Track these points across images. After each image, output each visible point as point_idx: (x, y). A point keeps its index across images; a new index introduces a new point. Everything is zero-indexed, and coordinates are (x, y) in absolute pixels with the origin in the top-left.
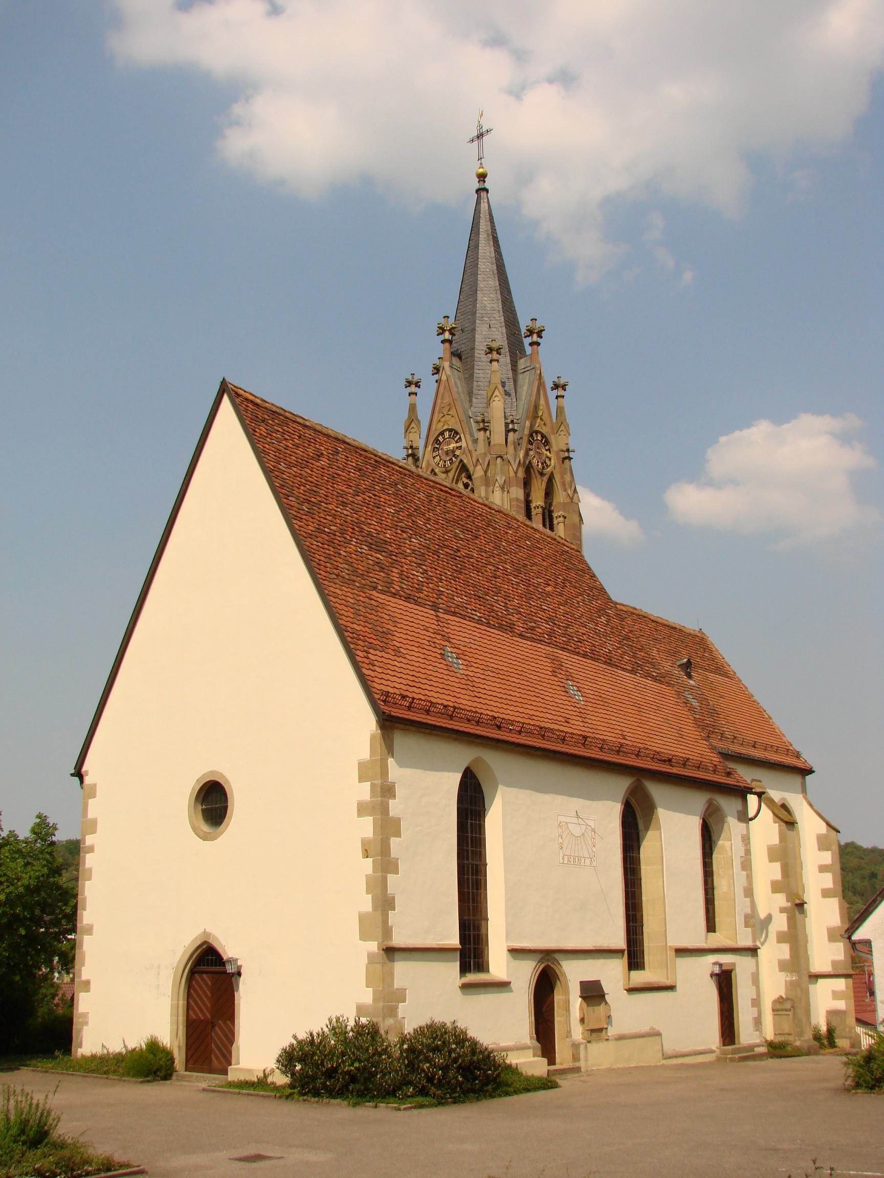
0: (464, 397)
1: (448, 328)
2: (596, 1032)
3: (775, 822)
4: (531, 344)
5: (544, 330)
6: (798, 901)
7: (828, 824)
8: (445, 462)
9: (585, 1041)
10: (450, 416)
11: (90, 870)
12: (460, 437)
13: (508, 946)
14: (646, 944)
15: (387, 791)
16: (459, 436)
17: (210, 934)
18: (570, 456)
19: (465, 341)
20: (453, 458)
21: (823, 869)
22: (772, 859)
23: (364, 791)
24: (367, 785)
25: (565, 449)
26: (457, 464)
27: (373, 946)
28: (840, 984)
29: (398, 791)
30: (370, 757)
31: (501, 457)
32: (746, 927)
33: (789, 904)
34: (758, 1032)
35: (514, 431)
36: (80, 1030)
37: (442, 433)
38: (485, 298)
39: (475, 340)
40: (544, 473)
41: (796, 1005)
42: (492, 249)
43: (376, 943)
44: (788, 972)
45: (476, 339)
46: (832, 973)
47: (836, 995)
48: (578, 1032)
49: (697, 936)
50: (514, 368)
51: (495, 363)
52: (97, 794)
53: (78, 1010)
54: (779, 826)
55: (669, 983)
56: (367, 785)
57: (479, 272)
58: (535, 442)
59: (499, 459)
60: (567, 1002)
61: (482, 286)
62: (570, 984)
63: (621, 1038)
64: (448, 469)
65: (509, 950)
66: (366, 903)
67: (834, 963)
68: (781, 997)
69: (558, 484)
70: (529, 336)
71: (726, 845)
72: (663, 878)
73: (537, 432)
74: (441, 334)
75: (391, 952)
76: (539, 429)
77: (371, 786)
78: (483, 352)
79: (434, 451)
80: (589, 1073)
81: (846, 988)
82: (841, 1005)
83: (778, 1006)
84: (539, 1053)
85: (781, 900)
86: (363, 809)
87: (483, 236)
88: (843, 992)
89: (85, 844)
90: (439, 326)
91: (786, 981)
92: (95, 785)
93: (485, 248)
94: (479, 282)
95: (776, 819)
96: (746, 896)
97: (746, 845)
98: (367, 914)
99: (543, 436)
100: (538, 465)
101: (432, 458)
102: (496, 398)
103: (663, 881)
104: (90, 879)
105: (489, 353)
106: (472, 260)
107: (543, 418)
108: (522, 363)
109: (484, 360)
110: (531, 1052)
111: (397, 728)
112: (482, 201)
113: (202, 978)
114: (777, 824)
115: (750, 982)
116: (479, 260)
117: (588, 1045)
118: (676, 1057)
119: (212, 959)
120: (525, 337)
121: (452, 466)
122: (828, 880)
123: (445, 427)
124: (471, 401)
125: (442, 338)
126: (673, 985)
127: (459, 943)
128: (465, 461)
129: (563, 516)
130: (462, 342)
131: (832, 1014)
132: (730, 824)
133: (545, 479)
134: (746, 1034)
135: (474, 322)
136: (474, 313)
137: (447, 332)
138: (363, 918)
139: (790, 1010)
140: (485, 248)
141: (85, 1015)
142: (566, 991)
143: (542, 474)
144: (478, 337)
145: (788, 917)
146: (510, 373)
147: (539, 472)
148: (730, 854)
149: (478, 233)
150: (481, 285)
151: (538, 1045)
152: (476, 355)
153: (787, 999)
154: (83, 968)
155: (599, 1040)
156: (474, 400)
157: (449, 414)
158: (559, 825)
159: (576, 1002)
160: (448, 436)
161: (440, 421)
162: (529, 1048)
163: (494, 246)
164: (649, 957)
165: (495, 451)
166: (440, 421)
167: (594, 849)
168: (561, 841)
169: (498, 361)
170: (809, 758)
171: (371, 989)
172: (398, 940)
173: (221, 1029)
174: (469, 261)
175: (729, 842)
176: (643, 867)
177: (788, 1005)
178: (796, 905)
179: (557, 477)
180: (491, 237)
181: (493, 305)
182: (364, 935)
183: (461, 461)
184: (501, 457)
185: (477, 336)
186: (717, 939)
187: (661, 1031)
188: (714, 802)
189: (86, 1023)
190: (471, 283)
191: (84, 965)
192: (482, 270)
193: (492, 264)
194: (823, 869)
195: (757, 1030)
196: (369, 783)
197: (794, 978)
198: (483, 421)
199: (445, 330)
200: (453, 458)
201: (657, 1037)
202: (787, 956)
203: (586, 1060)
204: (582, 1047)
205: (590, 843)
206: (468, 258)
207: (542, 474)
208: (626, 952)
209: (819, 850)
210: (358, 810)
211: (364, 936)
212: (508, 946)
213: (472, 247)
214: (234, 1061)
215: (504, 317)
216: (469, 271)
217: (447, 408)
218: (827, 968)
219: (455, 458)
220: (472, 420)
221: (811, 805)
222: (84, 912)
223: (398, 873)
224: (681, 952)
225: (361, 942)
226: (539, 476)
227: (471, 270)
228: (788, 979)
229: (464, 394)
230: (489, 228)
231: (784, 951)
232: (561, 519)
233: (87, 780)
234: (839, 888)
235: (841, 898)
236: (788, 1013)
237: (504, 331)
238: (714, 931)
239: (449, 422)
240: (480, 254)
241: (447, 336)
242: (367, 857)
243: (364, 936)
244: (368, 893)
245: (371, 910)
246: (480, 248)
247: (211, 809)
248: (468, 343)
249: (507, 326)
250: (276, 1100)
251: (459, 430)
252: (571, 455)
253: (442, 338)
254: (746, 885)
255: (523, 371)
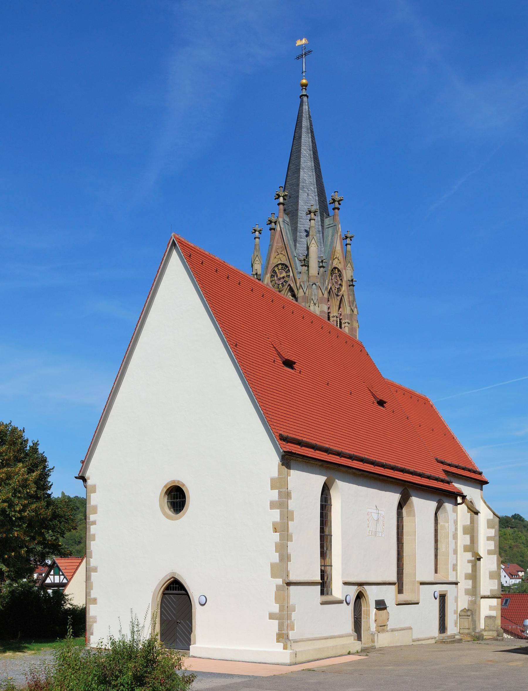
0: (292, 243)
1: (283, 195)
2: (382, 627)
3: (468, 512)
4: (334, 209)
5: (343, 200)
6: (478, 557)
7: (494, 514)
8: (278, 285)
9: (377, 632)
10: (282, 255)
11: (94, 535)
12: (289, 269)
13: (343, 581)
14: (404, 580)
15: (286, 495)
16: (288, 269)
17: (176, 573)
18: (353, 284)
19: (292, 204)
20: (284, 283)
21: (489, 539)
22: (465, 533)
23: (274, 495)
24: (276, 491)
25: (350, 279)
26: (287, 287)
27: (280, 581)
28: (495, 602)
29: (293, 495)
30: (278, 476)
31: (315, 284)
32: (453, 571)
33: (473, 558)
34: (456, 628)
35: (323, 267)
36: (91, 626)
37: (277, 266)
38: (305, 175)
39: (298, 204)
40: (339, 295)
41: (473, 613)
42: (310, 140)
43: (281, 580)
44: (470, 595)
45: (299, 204)
46: (490, 596)
47: (491, 608)
48: (373, 627)
49: (430, 577)
50: (322, 224)
51: (312, 221)
52: (96, 491)
53: (89, 614)
54: (471, 515)
55: (415, 600)
56: (276, 491)
57: (301, 156)
58: (334, 274)
59: (314, 285)
60: (368, 611)
61: (303, 166)
62: (370, 601)
63: (393, 630)
64: (280, 290)
65: (343, 583)
66: (275, 558)
67: (491, 591)
68: (465, 609)
69: (346, 301)
70: (332, 203)
71: (446, 525)
72: (415, 543)
73: (335, 268)
74: (277, 198)
75: (289, 584)
76: (337, 266)
77: (279, 492)
78: (305, 213)
79: (271, 277)
80: (381, 649)
81: (497, 604)
82: (493, 613)
83: (463, 614)
84: (356, 638)
85: (469, 556)
86: (273, 505)
87: (304, 130)
88: (495, 606)
89: (90, 520)
90: (277, 193)
91: (468, 600)
92: (95, 486)
93: (306, 139)
94: (301, 163)
95: (469, 510)
96: (454, 554)
97: (456, 525)
98: (276, 563)
99: (339, 270)
100: (335, 290)
101: (270, 282)
102: (313, 245)
103: (415, 545)
104: (94, 540)
105: (309, 214)
106: (297, 147)
107: (339, 258)
108: (327, 221)
109: (304, 218)
110: (352, 638)
111: (292, 459)
112: (304, 104)
113: (170, 597)
114: (470, 513)
115: (454, 601)
116: (302, 147)
117: (379, 634)
118: (418, 641)
119: (176, 587)
120: (330, 203)
121: (283, 288)
122: (492, 545)
123: (279, 262)
124: (295, 246)
125: (277, 201)
126: (418, 602)
127: (320, 579)
128: (292, 285)
129: (348, 323)
130: (290, 205)
131: (488, 618)
132: (449, 514)
133: (339, 298)
134: (452, 629)
135: (298, 192)
136: (298, 185)
137: (281, 197)
138: (273, 566)
139: (470, 616)
140: (306, 139)
141: (95, 617)
142: (368, 605)
143: (337, 295)
144: (301, 202)
145: (472, 565)
146: (320, 227)
147: (336, 294)
148: (448, 530)
149: (301, 127)
150: (303, 165)
151: (356, 634)
152: (299, 214)
153: (468, 610)
154: (92, 591)
155: (383, 631)
156: (297, 244)
157: (282, 254)
158: (368, 514)
159: (373, 610)
160: (281, 268)
161: (275, 258)
162: (352, 636)
163: (311, 137)
164: (406, 587)
165: (312, 280)
166: (275, 258)
167: (384, 527)
168: (368, 523)
169: (314, 220)
170: (486, 476)
171: (278, 605)
172: (293, 578)
173: (183, 625)
174: (295, 148)
175: (448, 524)
176: (404, 537)
177: (469, 613)
178: (477, 559)
179: (346, 297)
180: (310, 131)
181: (311, 180)
182: (274, 575)
183: (289, 285)
184: (315, 284)
185: (300, 201)
186: (440, 577)
187: (412, 627)
188: (442, 501)
189: (96, 622)
190: (296, 163)
191: (92, 589)
192: (304, 154)
193: (310, 151)
194: (489, 539)
195: (456, 627)
196: (278, 490)
197: (473, 599)
198: (352, 280)
199: (280, 196)
200: (284, 283)
201: (410, 630)
202: (470, 587)
203: (378, 642)
204: (376, 635)
205: (382, 524)
206: (294, 145)
207: (337, 295)
208: (397, 584)
209: (488, 528)
210: (270, 506)
211: (274, 576)
212: (343, 581)
213: (297, 138)
214: (192, 643)
215: (317, 188)
216: (295, 155)
217: (281, 250)
218: (488, 593)
219: (285, 283)
220: (296, 258)
221: (485, 503)
222: (91, 559)
223: (292, 541)
224: (422, 584)
225: (272, 579)
226: (335, 296)
227: (297, 154)
228: (470, 599)
229: (291, 240)
230: (309, 124)
231: (469, 584)
232: (347, 324)
233: (89, 482)
234: (498, 550)
235: (498, 555)
236: (469, 617)
237: (317, 198)
238: (437, 573)
239: (281, 259)
240: (302, 143)
241: (281, 200)
242: (276, 532)
243: (274, 576)
244: (276, 552)
245: (278, 561)
246: (302, 138)
247: (174, 502)
248: (294, 206)
249: (319, 195)
250: (448, 644)
251: (288, 265)
252: (354, 283)
253: (277, 201)
254: (454, 548)
255: (328, 226)
